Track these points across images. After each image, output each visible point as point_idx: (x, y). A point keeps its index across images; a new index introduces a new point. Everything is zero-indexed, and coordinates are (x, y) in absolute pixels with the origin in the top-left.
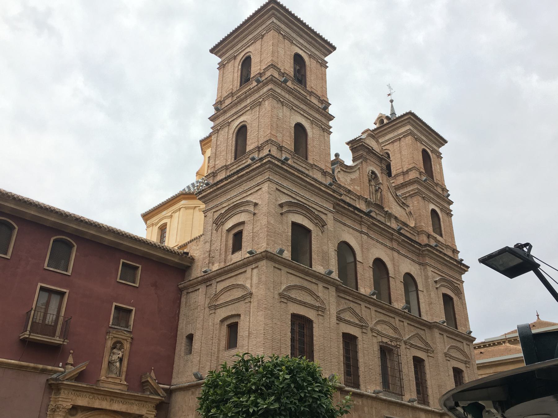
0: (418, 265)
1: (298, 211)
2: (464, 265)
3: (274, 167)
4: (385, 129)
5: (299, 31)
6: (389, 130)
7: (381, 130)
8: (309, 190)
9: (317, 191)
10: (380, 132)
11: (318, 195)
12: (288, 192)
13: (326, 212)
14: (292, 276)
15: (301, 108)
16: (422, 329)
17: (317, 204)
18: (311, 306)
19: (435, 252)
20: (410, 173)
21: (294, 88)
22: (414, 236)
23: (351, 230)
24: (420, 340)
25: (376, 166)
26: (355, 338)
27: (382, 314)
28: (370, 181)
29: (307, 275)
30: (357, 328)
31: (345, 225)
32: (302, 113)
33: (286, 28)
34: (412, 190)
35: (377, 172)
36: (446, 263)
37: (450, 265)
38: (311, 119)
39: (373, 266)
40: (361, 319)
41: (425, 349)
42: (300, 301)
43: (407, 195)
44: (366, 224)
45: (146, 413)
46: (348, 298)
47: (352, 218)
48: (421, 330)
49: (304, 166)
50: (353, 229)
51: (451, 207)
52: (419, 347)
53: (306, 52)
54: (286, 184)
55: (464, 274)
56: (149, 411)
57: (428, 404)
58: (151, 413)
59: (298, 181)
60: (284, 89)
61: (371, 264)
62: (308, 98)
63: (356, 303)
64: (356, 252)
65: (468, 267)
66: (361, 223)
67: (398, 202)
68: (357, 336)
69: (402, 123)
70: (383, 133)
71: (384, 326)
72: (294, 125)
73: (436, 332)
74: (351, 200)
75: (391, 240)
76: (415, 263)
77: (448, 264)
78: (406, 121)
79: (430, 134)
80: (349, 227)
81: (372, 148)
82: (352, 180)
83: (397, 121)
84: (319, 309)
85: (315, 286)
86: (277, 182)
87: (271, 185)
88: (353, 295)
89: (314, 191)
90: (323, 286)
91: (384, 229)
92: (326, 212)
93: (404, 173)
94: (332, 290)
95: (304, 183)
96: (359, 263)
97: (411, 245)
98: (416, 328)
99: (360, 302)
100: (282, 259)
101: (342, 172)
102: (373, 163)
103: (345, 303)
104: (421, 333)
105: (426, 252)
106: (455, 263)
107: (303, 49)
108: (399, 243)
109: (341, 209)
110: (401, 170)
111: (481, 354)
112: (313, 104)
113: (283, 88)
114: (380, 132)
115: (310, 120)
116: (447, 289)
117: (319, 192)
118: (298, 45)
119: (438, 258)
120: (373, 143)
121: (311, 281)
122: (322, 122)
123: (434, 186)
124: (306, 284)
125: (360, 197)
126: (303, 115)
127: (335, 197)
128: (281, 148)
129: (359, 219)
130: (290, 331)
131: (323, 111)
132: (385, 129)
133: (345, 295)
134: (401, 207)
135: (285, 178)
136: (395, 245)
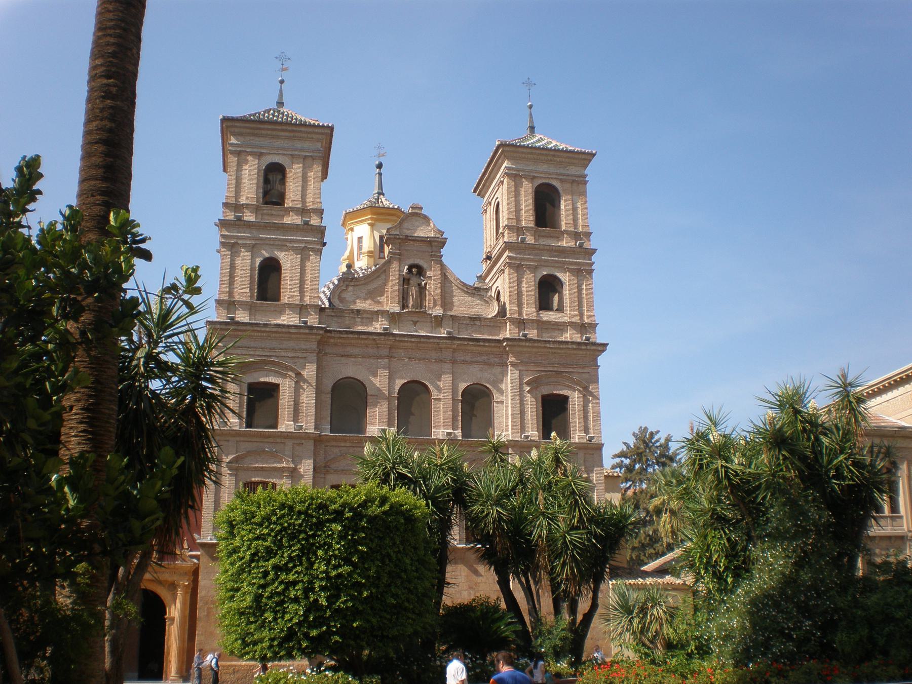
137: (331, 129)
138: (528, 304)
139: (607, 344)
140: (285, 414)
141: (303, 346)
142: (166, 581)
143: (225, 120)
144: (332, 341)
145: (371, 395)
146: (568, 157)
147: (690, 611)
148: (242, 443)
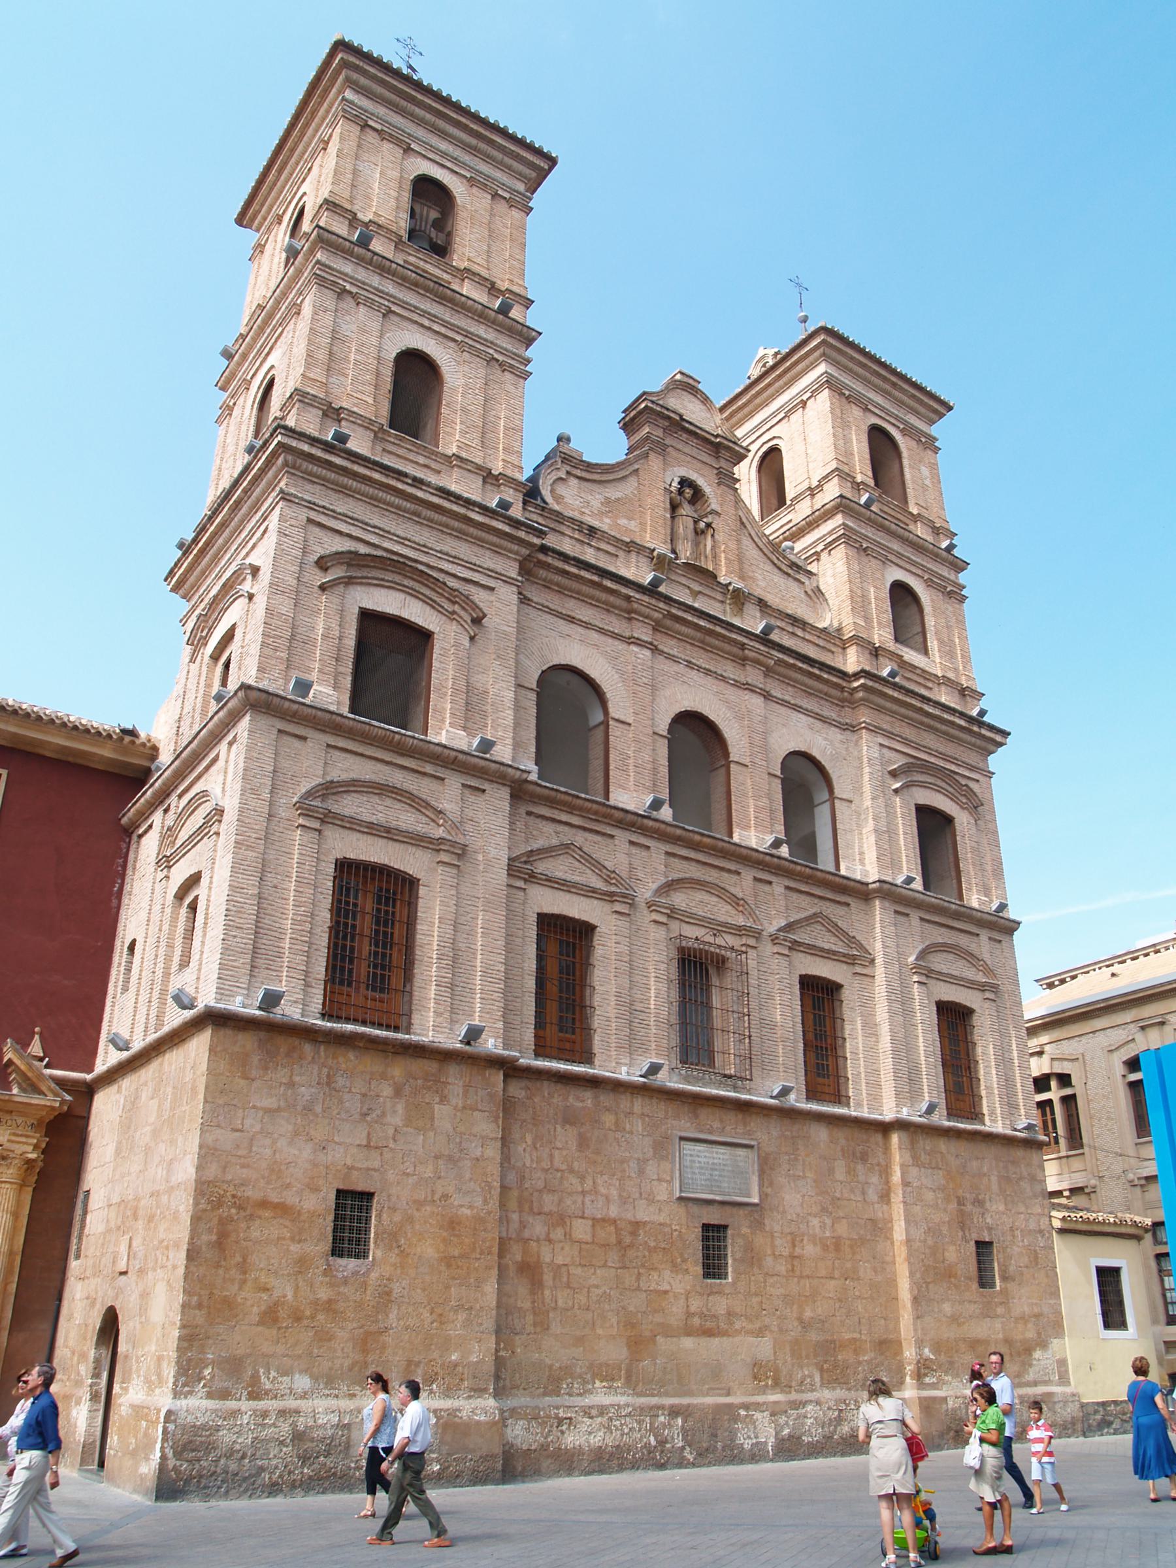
0: (837, 730)
1: (383, 580)
2: (992, 728)
3: (299, 461)
4: (769, 385)
5: (433, 119)
6: (777, 385)
7: (758, 388)
8: (430, 524)
9: (456, 524)
10: (759, 394)
11: (461, 536)
12: (352, 528)
13: (491, 583)
14: (348, 756)
15: (422, 310)
16: (839, 903)
17: (455, 560)
18: (412, 838)
19: (890, 692)
20: (825, 487)
21: (405, 261)
22: (830, 654)
23: (594, 635)
24: (830, 931)
25: (699, 465)
26: (583, 932)
27: (694, 864)
28: (674, 507)
29: (402, 755)
30: (596, 902)
31: (571, 619)
32: (426, 323)
33: (392, 113)
34: (830, 533)
35: (701, 482)
36: (932, 723)
37: (944, 728)
38: (459, 338)
39: (669, 731)
40: (610, 876)
41: (845, 955)
42: (371, 825)
43: (819, 548)
44: (646, 617)
45: (9, 1141)
46: (564, 817)
47: (598, 601)
48: (834, 906)
49: (422, 460)
50: (602, 631)
51: (962, 578)
52: (829, 951)
53: (456, 173)
54: (343, 505)
55: (993, 752)
56: (15, 1134)
57: (977, 1116)
58: (24, 1139)
59: (389, 498)
60: (361, 261)
61: (663, 726)
62: (455, 287)
63: (597, 832)
64: (608, 695)
65: (1006, 734)
66: (629, 614)
67: (776, 561)
68: (593, 921)
69: (807, 362)
70: (765, 395)
71: (701, 896)
72: (394, 355)
73: (879, 910)
74: (601, 554)
75: (743, 661)
76: (826, 725)
77: (938, 725)
78: (817, 354)
79: (894, 385)
80: (587, 625)
81: (681, 416)
82: (607, 501)
83: (795, 358)
84: (442, 847)
85: (434, 785)
86: (309, 502)
87: (287, 511)
88: (581, 809)
89: (447, 526)
90: (463, 785)
91: (711, 633)
92: (491, 583)
93: (812, 492)
94: (499, 797)
95: (409, 505)
96: (617, 724)
97: (811, 675)
98: (816, 901)
99: (609, 830)
100: (302, 707)
101: (573, 482)
102: (689, 459)
103: (557, 833)
104: (830, 910)
105: (861, 694)
106: (962, 723)
107: (449, 164)
108: (768, 672)
109: (558, 578)
110: (805, 485)
111: (1114, 979)
112: (463, 299)
113: (360, 259)
114: (759, 394)
115: (455, 341)
116: (933, 793)
117: (464, 526)
118: (431, 156)
119: (903, 710)
120: (690, 406)
121: (420, 769)
122: (496, 345)
123: (907, 521)
124: (398, 778)
125: (631, 547)
126: (429, 329)
127: (521, 542)
128: (339, 415)
129: (624, 604)
130: (329, 906)
131: (501, 317)
132: (769, 385)
133: (556, 812)
134: (788, 575)
135: (343, 491)
136: (754, 676)
137: (553, 162)
138: (879, 623)
139: (1009, 734)
140: (444, 709)
141: (489, 560)
142: (579, 1451)
143: (341, 45)
144: (542, 573)
145: (617, 720)
146: (913, 397)
147: (219, 1131)
148: (337, 753)
